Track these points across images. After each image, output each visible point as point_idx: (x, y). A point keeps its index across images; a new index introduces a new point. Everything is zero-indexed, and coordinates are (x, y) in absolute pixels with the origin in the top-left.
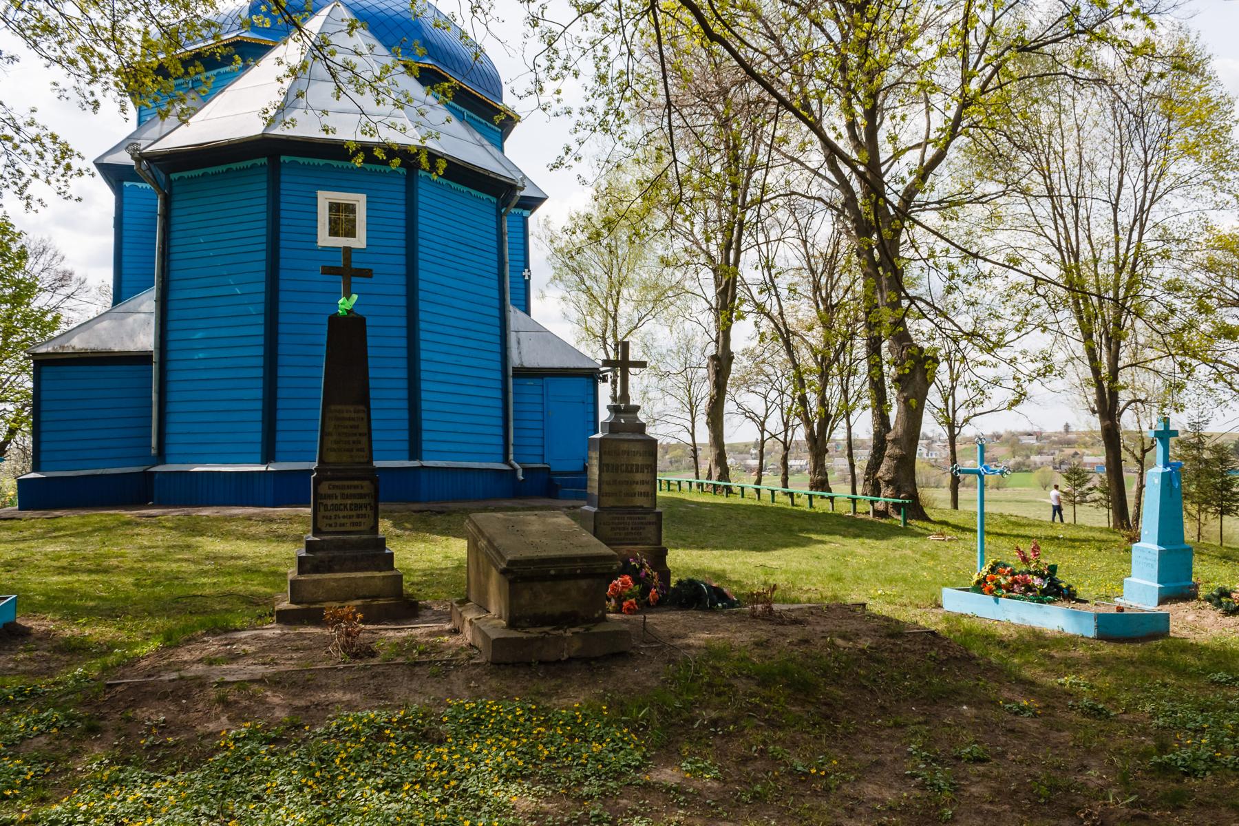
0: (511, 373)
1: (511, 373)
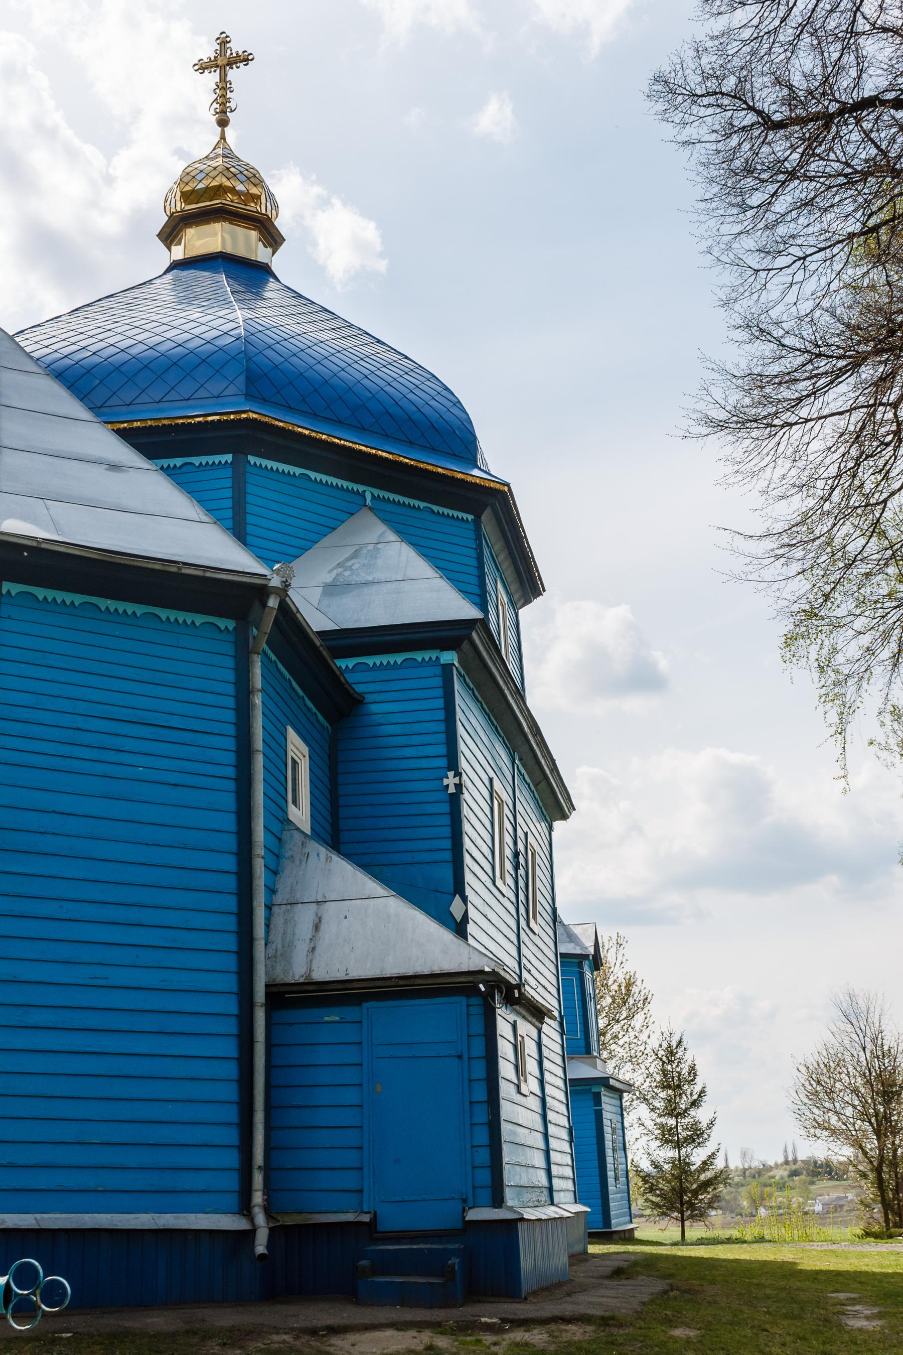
0: (260, 995)
1: (260, 995)
